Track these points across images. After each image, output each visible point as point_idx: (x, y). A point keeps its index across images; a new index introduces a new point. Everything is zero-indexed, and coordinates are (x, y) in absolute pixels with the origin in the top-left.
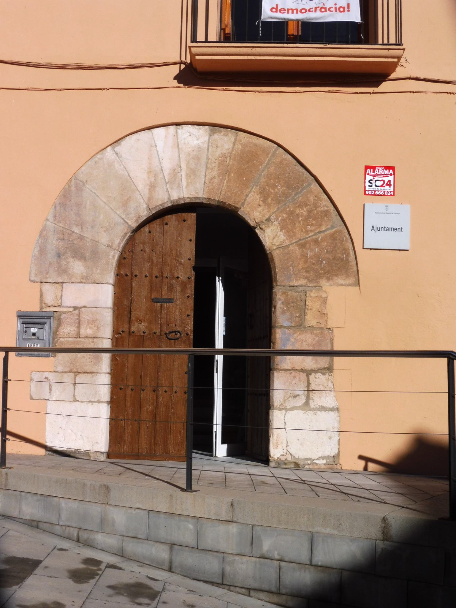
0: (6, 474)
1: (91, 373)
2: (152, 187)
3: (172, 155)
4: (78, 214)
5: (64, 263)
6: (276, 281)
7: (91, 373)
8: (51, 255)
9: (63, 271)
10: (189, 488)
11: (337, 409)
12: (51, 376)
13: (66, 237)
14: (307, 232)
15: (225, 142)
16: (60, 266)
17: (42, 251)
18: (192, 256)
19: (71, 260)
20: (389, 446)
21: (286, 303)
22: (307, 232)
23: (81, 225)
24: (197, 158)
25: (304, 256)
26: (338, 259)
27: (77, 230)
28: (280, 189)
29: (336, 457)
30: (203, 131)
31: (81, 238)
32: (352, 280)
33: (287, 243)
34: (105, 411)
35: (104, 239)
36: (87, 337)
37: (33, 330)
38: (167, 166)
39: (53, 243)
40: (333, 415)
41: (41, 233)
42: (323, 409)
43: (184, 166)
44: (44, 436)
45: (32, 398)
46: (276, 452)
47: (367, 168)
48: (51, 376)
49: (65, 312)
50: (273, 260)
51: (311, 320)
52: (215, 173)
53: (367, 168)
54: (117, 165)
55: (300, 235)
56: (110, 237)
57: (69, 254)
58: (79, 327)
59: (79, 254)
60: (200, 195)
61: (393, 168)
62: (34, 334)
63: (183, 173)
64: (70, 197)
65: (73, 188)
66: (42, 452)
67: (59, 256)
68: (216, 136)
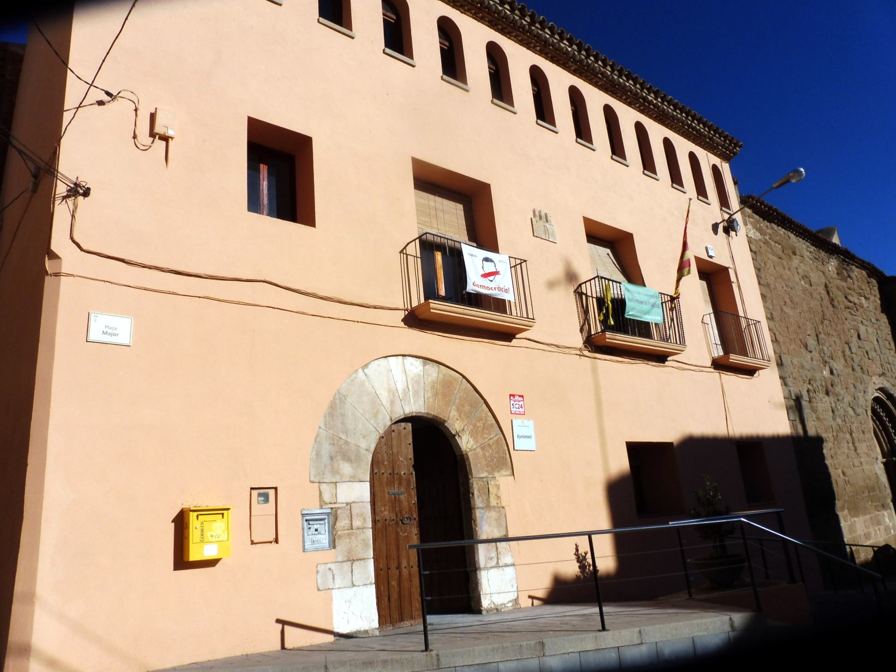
0: (438, 655)
1: (364, 559)
2: (392, 403)
3: (399, 378)
4: (343, 423)
5: (335, 465)
6: (472, 475)
7: (364, 559)
8: (325, 458)
9: (335, 472)
10: (604, 629)
11: (514, 565)
12: (333, 566)
13: (336, 442)
14: (484, 439)
15: (432, 369)
16: (333, 468)
17: (318, 454)
18: (411, 455)
19: (341, 462)
20: (542, 586)
21: (479, 491)
22: (484, 439)
23: (346, 432)
24: (418, 382)
25: (484, 455)
26: (503, 458)
27: (344, 437)
28: (467, 408)
29: (516, 601)
30: (418, 363)
31: (347, 443)
32: (510, 472)
33: (475, 447)
34: (372, 589)
35: (363, 444)
36: (358, 528)
37: (315, 527)
38: (400, 387)
39: (326, 449)
40: (511, 569)
41: (316, 437)
42: (506, 566)
43: (410, 387)
44: (332, 623)
45: (319, 590)
46: (485, 603)
47: (511, 395)
48: (333, 566)
49: (339, 508)
50: (468, 458)
51: (493, 502)
52: (430, 394)
53: (511, 395)
54: (367, 384)
55: (481, 441)
56: (366, 444)
57: (339, 457)
58: (351, 521)
59: (347, 458)
60: (423, 411)
61: (522, 396)
62: (316, 530)
63: (411, 393)
64: (335, 409)
65: (337, 401)
66: (330, 638)
67: (332, 458)
68: (427, 367)
